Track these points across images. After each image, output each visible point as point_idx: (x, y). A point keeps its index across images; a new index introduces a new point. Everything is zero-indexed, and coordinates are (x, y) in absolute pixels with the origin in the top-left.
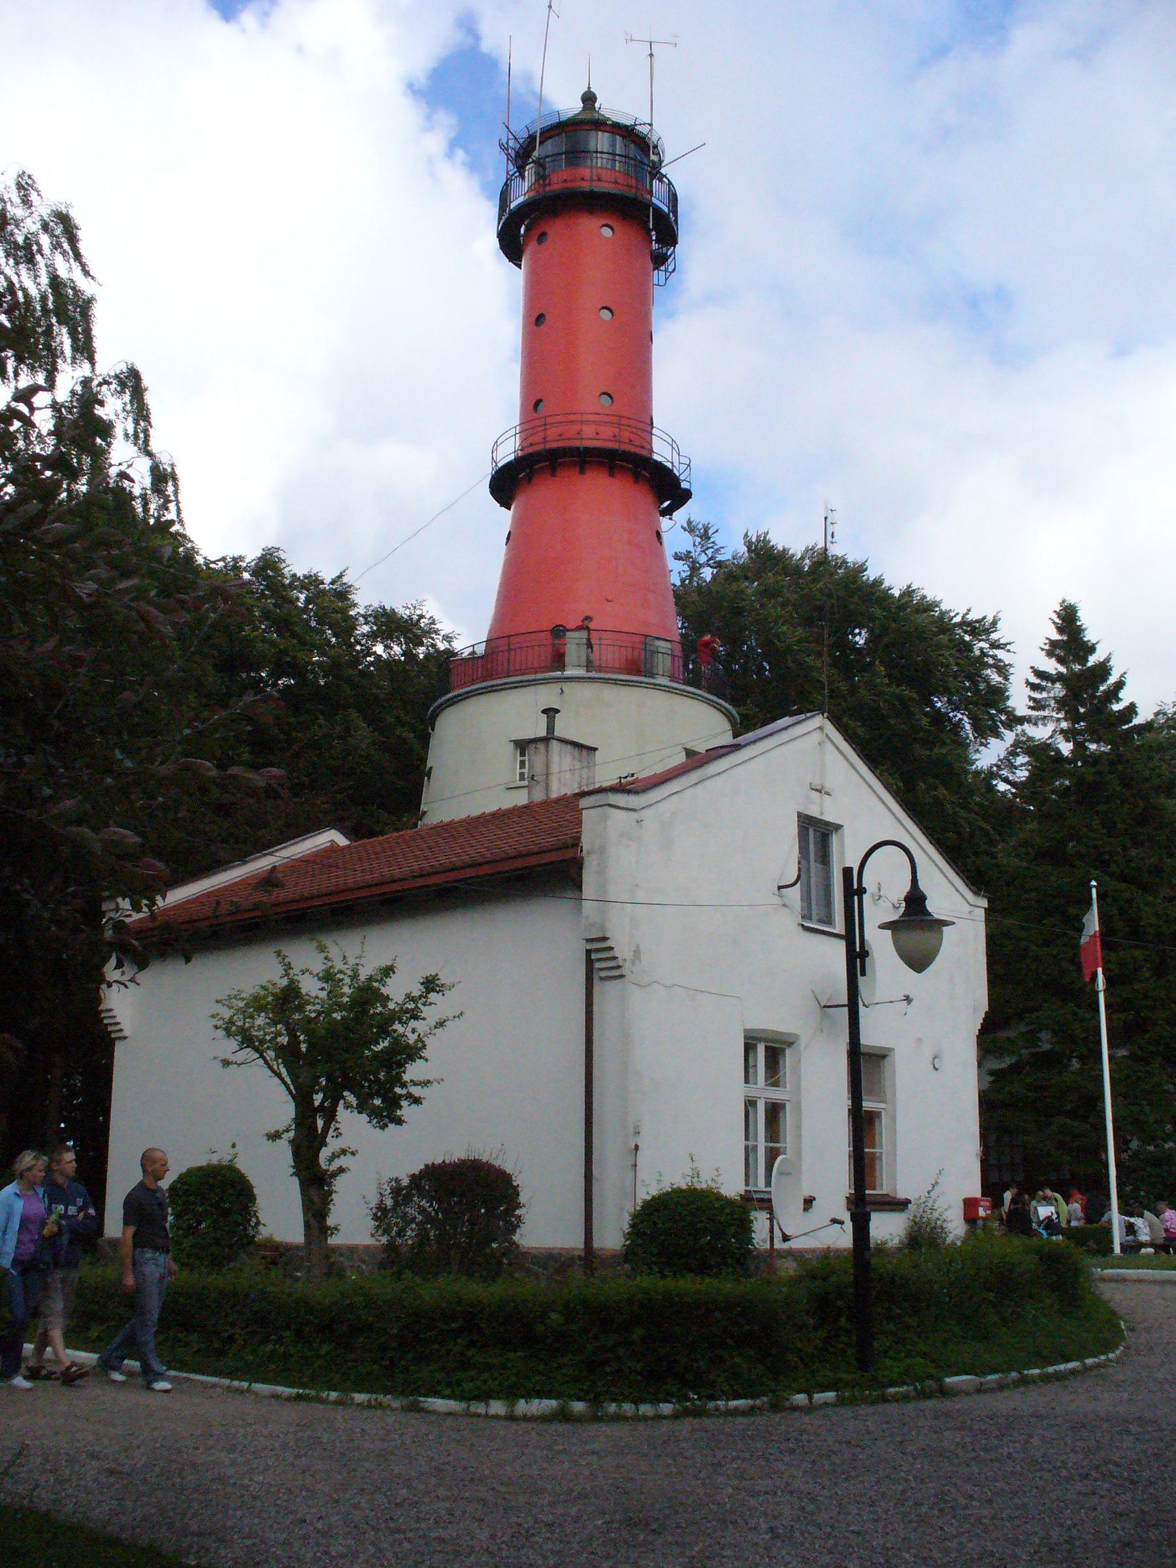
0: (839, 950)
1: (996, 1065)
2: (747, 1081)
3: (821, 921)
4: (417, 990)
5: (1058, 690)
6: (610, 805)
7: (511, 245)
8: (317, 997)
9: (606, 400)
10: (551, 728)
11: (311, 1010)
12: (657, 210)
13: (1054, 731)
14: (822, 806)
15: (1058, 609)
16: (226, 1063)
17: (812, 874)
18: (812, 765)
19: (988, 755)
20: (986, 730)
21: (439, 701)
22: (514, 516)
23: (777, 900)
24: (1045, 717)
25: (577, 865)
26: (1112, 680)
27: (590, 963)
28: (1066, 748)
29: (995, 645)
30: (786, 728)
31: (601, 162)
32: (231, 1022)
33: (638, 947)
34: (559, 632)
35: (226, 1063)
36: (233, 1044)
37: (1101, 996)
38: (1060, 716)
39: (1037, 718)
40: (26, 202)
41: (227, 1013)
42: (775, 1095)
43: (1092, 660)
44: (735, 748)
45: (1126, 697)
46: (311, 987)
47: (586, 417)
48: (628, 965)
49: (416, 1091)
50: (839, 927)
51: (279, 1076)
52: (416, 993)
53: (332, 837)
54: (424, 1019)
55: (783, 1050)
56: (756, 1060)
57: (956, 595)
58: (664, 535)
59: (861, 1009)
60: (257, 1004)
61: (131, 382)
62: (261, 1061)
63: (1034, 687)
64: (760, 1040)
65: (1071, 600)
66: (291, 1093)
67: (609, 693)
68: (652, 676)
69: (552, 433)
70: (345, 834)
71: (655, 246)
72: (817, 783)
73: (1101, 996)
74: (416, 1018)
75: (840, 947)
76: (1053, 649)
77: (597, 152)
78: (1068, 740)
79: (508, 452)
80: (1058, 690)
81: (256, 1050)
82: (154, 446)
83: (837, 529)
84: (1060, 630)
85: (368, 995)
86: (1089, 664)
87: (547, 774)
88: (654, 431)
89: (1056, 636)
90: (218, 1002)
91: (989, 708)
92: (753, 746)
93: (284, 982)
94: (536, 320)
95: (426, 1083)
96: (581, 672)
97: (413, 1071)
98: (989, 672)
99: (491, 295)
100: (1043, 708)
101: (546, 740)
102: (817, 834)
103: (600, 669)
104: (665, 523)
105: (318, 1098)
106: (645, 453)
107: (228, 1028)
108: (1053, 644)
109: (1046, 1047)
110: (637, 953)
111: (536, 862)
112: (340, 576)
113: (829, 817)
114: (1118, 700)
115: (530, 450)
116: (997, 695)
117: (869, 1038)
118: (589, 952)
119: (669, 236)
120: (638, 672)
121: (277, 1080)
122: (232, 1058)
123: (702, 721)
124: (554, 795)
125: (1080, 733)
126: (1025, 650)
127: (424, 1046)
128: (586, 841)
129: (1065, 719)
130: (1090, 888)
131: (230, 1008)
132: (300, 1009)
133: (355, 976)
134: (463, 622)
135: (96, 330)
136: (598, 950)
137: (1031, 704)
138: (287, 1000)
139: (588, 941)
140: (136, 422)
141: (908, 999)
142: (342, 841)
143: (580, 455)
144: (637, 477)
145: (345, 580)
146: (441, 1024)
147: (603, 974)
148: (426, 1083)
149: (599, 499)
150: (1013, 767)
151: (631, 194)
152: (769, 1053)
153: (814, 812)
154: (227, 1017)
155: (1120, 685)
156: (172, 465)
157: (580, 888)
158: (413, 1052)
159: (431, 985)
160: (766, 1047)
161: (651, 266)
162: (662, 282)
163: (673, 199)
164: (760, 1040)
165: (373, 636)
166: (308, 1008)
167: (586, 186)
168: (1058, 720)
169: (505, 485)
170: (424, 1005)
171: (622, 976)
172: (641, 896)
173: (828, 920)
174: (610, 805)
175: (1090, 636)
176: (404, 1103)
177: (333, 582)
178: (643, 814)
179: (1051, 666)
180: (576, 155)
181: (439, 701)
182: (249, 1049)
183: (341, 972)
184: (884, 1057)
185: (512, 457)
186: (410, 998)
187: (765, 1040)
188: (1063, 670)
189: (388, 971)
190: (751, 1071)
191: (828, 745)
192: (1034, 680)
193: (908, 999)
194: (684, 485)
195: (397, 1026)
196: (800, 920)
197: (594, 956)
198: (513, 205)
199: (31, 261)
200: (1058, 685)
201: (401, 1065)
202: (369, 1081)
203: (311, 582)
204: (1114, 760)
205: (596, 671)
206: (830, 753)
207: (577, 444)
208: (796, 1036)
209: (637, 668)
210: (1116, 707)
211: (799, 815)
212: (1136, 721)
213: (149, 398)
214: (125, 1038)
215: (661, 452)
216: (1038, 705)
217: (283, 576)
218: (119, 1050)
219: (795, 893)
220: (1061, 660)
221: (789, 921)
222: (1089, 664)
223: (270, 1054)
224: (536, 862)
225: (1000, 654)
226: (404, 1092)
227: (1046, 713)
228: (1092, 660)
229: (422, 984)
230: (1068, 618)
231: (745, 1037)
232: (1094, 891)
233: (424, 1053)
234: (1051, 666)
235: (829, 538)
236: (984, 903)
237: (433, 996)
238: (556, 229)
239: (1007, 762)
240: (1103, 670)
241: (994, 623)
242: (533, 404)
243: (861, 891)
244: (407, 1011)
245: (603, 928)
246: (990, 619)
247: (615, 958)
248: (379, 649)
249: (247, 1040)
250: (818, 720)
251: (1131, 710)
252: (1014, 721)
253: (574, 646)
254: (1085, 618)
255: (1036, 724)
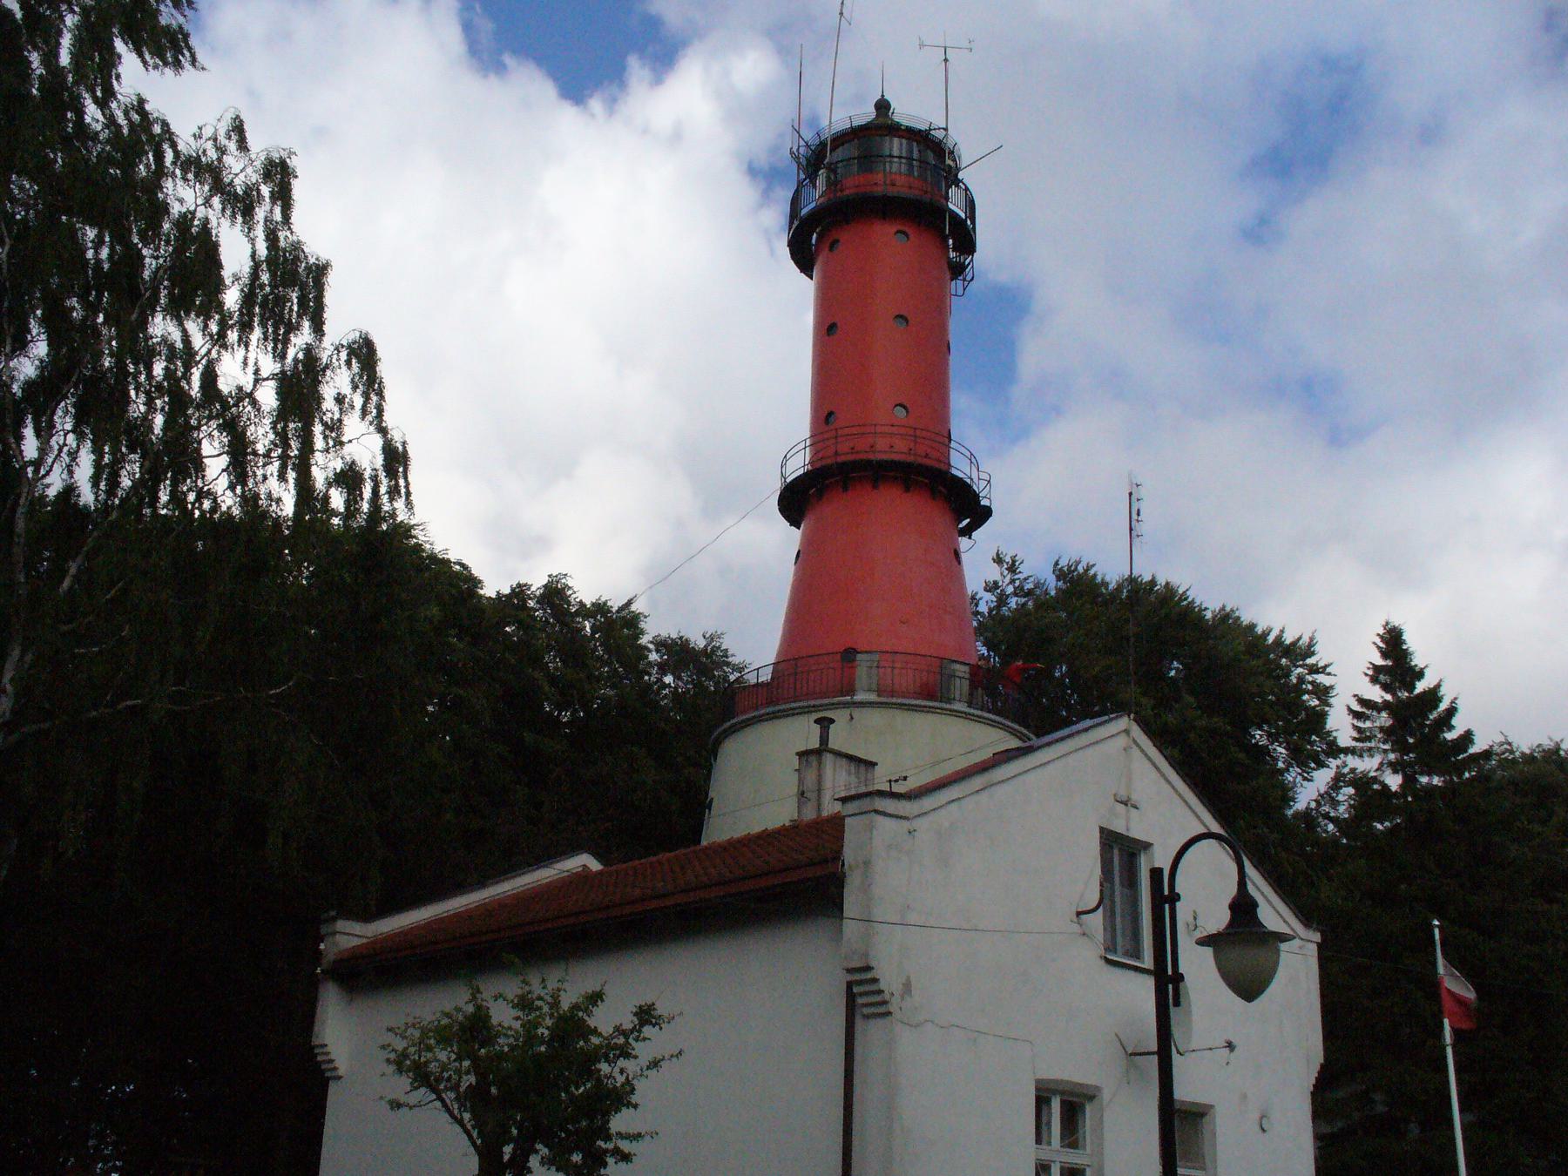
0: (1142, 991)
1: (1326, 1129)
2: (1039, 1141)
3: (1126, 954)
4: (628, 1022)
5: (1384, 719)
6: (876, 812)
7: (803, 257)
8: (510, 1028)
9: (900, 412)
10: (824, 739)
11: (503, 1043)
12: (953, 215)
13: (1381, 764)
14: (1128, 820)
15: (1381, 631)
16: (396, 1105)
17: (1118, 899)
18: (1115, 776)
19: (1308, 790)
20: (1306, 759)
21: (721, 729)
22: (804, 535)
23: (1076, 928)
24: (1370, 749)
25: (838, 881)
26: (1443, 706)
27: (851, 998)
28: (1394, 781)
29: (1314, 670)
30: (1086, 730)
31: (895, 166)
32: (404, 1055)
33: (908, 979)
34: (849, 654)
35: (396, 1105)
36: (405, 1082)
37: (1449, 1050)
38: (1387, 747)
39: (1362, 749)
40: (243, 145)
41: (400, 1045)
42: (1074, 1158)
43: (1420, 687)
44: (1029, 750)
45: (1460, 725)
46: (503, 1015)
47: (878, 429)
48: (895, 1001)
49: (625, 1146)
50: (1148, 962)
51: (460, 1122)
52: (628, 1026)
53: (586, 861)
54: (636, 1057)
55: (1082, 1107)
56: (1050, 1114)
57: (1276, 615)
58: (964, 557)
59: (1176, 1059)
60: (443, 1036)
61: (364, 353)
62: (438, 1104)
63: (1357, 715)
64: (1055, 1092)
65: (1396, 622)
66: (474, 1144)
67: (900, 717)
68: (949, 701)
69: (844, 447)
70: (597, 856)
71: (952, 254)
72: (1123, 794)
73: (1449, 1050)
74: (627, 1055)
75: (1150, 982)
76: (1376, 675)
77: (891, 156)
78: (1395, 772)
79: (798, 465)
80: (1384, 719)
81: (434, 1090)
82: (389, 419)
83: (1144, 506)
84: (1384, 655)
85: (572, 1026)
86: (1417, 691)
87: (819, 790)
88: (953, 444)
89: (1380, 662)
90: (390, 1030)
91: (1305, 729)
92: (1046, 750)
93: (470, 1009)
94: (827, 329)
95: (637, 1137)
96: (873, 697)
97: (620, 1122)
98: (1306, 697)
99: (782, 310)
100: (1369, 739)
101: (818, 752)
102: (1120, 851)
103: (892, 694)
104: (964, 543)
105: (508, 1150)
106: (943, 467)
107: (399, 1063)
108: (1376, 668)
109: (1381, 1109)
110: (907, 987)
111: (799, 881)
112: (629, 603)
113: (1137, 833)
114: (1451, 728)
115: (818, 465)
116: (1317, 719)
117: (1183, 1092)
118: (850, 985)
119: (967, 243)
120: (931, 696)
121: (458, 1128)
122: (403, 1099)
123: (991, 738)
124: (825, 814)
125: (1411, 764)
126: (1349, 675)
127: (633, 1090)
128: (849, 854)
129: (1393, 751)
130: (1431, 928)
131: (404, 1038)
132: (488, 1041)
133: (555, 1004)
134: (756, 647)
135: (329, 298)
136: (861, 983)
137: (1355, 734)
138: (473, 1030)
139: (849, 971)
140: (367, 398)
141: (1230, 1046)
142: (595, 865)
143: (876, 470)
144: (933, 493)
145: (633, 608)
146: (655, 1064)
147: (866, 1011)
148: (637, 1137)
149: (892, 519)
150: (1335, 803)
151: (926, 198)
152: (1065, 1108)
153: (1119, 826)
154: (400, 1048)
155: (1451, 711)
156: (404, 443)
157: (841, 909)
158: (620, 1098)
159: (646, 1015)
160: (1063, 1102)
161: (948, 275)
162: (960, 292)
163: (971, 205)
164: (1055, 1092)
165: (663, 668)
166: (501, 1041)
167: (879, 191)
168: (1385, 751)
169: (796, 501)
170: (637, 1040)
171: (889, 1013)
172: (912, 918)
173: (1136, 953)
174: (876, 812)
175: (1418, 661)
176: (610, 1160)
177: (621, 609)
178: (917, 823)
179: (1376, 694)
180: (869, 159)
181: (721, 729)
182: (423, 1090)
183: (540, 998)
184: (1202, 1115)
185: (801, 472)
186: (619, 1030)
187: (1062, 1093)
188: (1389, 697)
189: (595, 998)
190: (1044, 1128)
191: (1136, 752)
192: (1356, 707)
193: (1230, 1046)
194: (984, 502)
195: (604, 1067)
196: (1102, 952)
197: (855, 990)
198: (804, 212)
199: (248, 213)
200: (1384, 714)
201: (606, 1115)
202: (567, 1131)
203: (600, 608)
204: (1449, 792)
205: (889, 697)
206: (1140, 766)
207: (871, 457)
208: (1098, 1088)
209: (931, 694)
210: (1450, 736)
211: (1102, 830)
212: (1472, 751)
213: (383, 369)
214: (340, 1078)
215: (960, 467)
216: (1362, 735)
217: (569, 603)
218: (333, 1088)
219: (1096, 921)
220: (1386, 688)
221: (1090, 952)
222: (1417, 691)
223: (449, 1096)
224: (799, 881)
225: (1320, 678)
226: (610, 1146)
227: (1373, 744)
228: (1420, 687)
229: (636, 1014)
230: (1393, 642)
231: (1037, 1089)
232: (1437, 931)
233: (634, 1099)
234: (1376, 694)
235: (1134, 516)
236: (1317, 937)
237: (647, 1031)
238: (848, 236)
239: (1329, 797)
240: (1433, 696)
241: (1311, 645)
242: (825, 417)
243: (1174, 898)
244: (616, 1047)
245: (866, 955)
246: (1305, 640)
247: (880, 992)
248: (668, 679)
249: (423, 1077)
250: (1124, 722)
251: (1467, 738)
252: (1334, 750)
253: (864, 671)
254: (1411, 641)
255: (1361, 756)
